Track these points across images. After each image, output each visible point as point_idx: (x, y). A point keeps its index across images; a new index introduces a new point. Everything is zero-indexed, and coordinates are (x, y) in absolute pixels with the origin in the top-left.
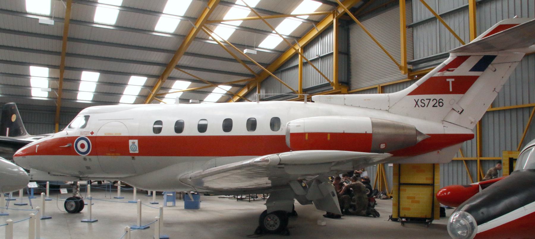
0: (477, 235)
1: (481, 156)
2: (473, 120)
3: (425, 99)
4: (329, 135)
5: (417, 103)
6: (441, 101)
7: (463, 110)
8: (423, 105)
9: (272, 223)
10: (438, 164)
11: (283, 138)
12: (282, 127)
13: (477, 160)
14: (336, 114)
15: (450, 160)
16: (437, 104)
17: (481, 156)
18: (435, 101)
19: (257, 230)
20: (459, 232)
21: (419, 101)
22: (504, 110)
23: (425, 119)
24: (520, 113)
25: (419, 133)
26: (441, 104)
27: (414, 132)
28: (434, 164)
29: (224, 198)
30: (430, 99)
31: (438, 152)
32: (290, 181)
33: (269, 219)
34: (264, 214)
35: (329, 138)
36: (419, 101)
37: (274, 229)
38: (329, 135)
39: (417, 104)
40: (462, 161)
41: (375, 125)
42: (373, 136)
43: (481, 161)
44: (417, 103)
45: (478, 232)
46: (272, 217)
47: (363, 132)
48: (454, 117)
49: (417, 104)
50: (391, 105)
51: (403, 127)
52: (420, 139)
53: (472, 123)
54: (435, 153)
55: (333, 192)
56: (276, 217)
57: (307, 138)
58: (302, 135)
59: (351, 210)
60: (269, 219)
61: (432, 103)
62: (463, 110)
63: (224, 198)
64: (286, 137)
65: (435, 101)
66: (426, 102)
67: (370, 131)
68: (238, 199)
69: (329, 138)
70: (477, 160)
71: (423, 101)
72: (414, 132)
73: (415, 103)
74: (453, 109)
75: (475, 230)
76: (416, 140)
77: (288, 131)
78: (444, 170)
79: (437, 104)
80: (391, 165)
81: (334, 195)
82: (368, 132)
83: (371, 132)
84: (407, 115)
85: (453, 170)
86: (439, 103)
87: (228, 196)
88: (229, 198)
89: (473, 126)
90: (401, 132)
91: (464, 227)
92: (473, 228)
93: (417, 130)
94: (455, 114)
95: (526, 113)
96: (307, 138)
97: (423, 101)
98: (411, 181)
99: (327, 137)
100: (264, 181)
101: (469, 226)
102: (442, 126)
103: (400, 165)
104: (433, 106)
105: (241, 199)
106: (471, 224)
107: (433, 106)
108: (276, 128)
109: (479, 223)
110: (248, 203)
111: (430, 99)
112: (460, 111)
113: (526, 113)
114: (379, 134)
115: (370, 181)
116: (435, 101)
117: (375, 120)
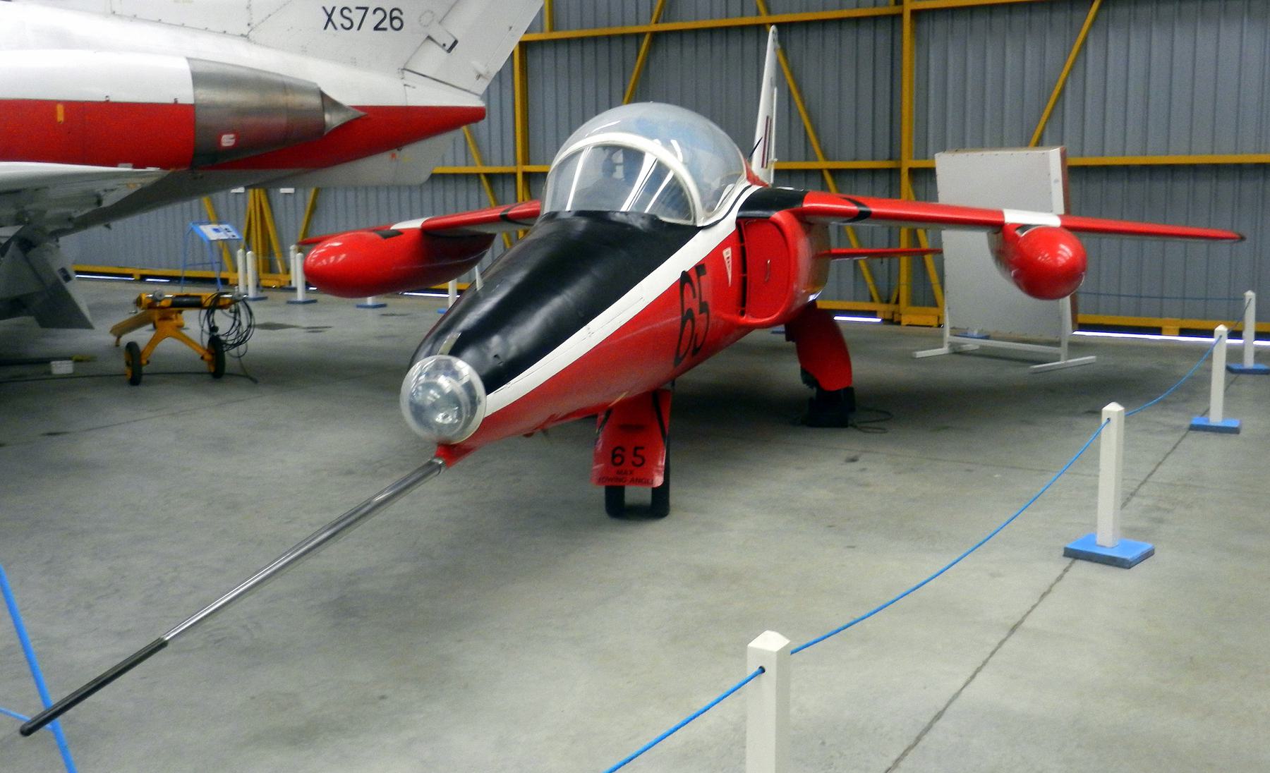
0: (486, 420)
1: (527, 161)
2: (482, 70)
3: (353, 9)
4: (60, 109)
5: (330, 16)
6: (395, 14)
7: (456, 42)
8: (347, 24)
13: (515, 175)
14: (87, 45)
16: (386, 24)
17: (527, 161)
18: (380, 15)
20: (439, 418)
23: (354, 62)
25: (328, 103)
26: (396, 23)
27: (315, 101)
30: (366, 9)
31: (393, 156)
35: (60, 117)
38: (60, 109)
39: (330, 20)
40: (478, 175)
41: (199, 79)
43: (527, 176)
44: (330, 16)
45: (488, 413)
48: (432, 59)
49: (330, 20)
50: (255, 21)
51: (285, 87)
52: (332, 120)
53: (479, 76)
61: (372, 19)
62: (456, 42)
65: (379, 12)
66: (356, 16)
67: (186, 95)
69: (60, 117)
70: (515, 175)
72: (315, 101)
73: (326, 18)
74: (429, 38)
75: (480, 408)
76: (323, 124)
78: (445, 203)
79: (386, 24)
82: (180, 101)
83: (190, 101)
84: (304, 51)
85: (456, 201)
86: (392, 19)
89: (482, 86)
90: (281, 99)
91: (452, 399)
92: (474, 402)
93: (323, 96)
98: (1132, 51)
99: (54, 112)
101: (464, 397)
102: (400, 84)
104: (376, 28)
106: (469, 387)
107: (376, 28)
109: (494, 381)
111: (366, 9)
112: (448, 47)
113: (630, 46)
116: (380, 15)
117: (201, 68)
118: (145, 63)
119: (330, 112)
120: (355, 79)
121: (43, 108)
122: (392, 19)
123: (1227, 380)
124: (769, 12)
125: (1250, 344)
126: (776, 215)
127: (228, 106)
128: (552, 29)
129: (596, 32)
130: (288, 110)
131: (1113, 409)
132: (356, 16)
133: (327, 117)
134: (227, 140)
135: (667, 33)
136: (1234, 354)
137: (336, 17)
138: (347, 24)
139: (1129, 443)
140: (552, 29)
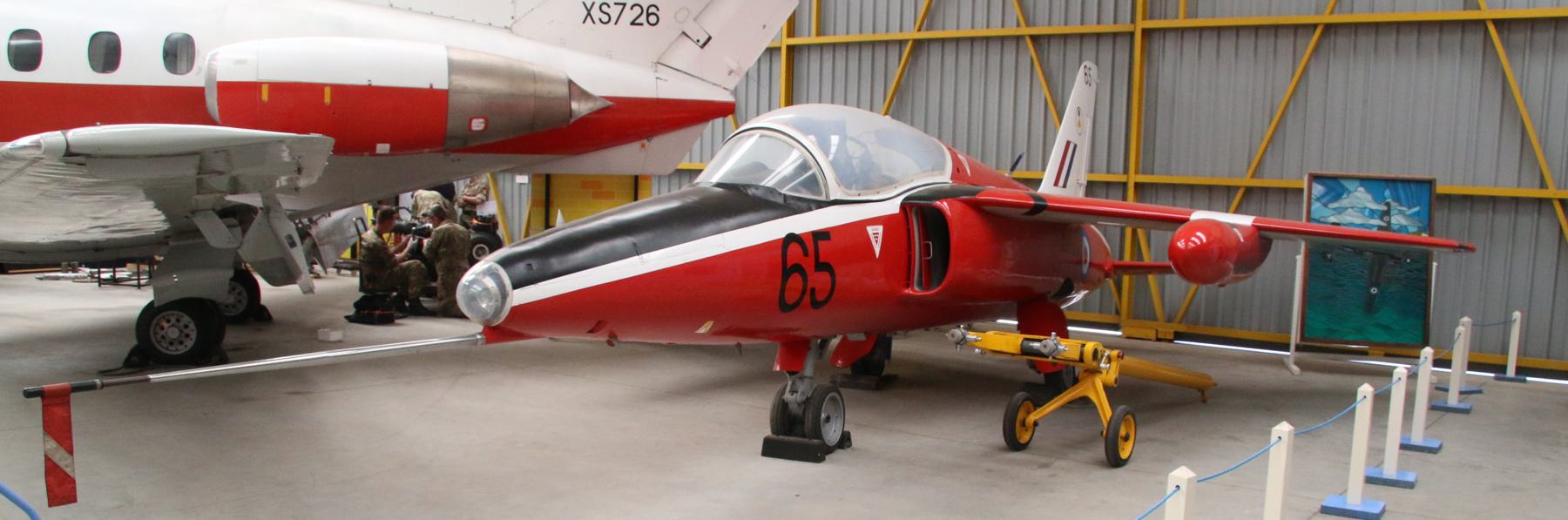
2: (734, 66)
4: (327, 91)
5: (589, 11)
6: (652, 10)
8: (605, 18)
9: (173, 333)
10: (647, 178)
11: (197, 94)
12: (196, 65)
15: (671, 170)
18: (637, 10)
19: (133, 352)
21: (596, 7)
22: (847, 45)
23: (609, 56)
24: (880, 53)
26: (653, 19)
27: (564, 90)
28: (636, 178)
29: (57, 278)
32: (193, 212)
33: (165, 325)
34: (149, 312)
35: (327, 100)
36: (596, 7)
37: (182, 350)
38: (327, 91)
41: (454, 68)
42: (452, 99)
44: (589, 11)
45: (515, 303)
46: (173, 320)
47: (423, 84)
48: (686, 54)
51: (534, 77)
52: (580, 108)
54: (634, 147)
55: (290, 237)
56: (186, 319)
57: (265, 96)
58: (253, 87)
59: (427, 303)
60: (165, 325)
61: (629, 15)
63: (57, 278)
64: (207, 92)
66: (614, 11)
67: (441, 84)
68: (106, 281)
69: (327, 100)
70: (1125, 185)
71: (605, 8)
77: (210, 77)
79: (643, 19)
80: (522, 179)
81: (293, 244)
83: (445, 86)
84: (563, 43)
86: (648, 15)
87: (70, 274)
88: (73, 279)
89: (732, 82)
90: (530, 88)
92: (504, 296)
93: (570, 83)
94: (690, 48)
95: (894, 52)
96: (265, 96)
97: (605, 8)
100: (142, 216)
102: (653, 76)
103: (548, 177)
104: (633, 23)
105: (114, 281)
107: (633, 23)
108: (182, 65)
110: (135, 291)
114: (465, 91)
115: (496, 225)
116: (637, 10)
117: (458, 56)
118: (404, 51)
119: (579, 100)
120: (607, 70)
121: (311, 91)
122: (650, 15)
123: (1427, 419)
124: (1028, 25)
125: (1457, 375)
126: (945, 205)
127: (480, 92)
128: (818, 34)
129: (1283, 184)
130: (536, 97)
131: (1283, 428)
132: (614, 11)
133: (574, 106)
134: (478, 125)
135: (930, 41)
136: (1440, 388)
137: (596, 13)
138: (605, 18)
139: (1296, 449)
140: (818, 34)
